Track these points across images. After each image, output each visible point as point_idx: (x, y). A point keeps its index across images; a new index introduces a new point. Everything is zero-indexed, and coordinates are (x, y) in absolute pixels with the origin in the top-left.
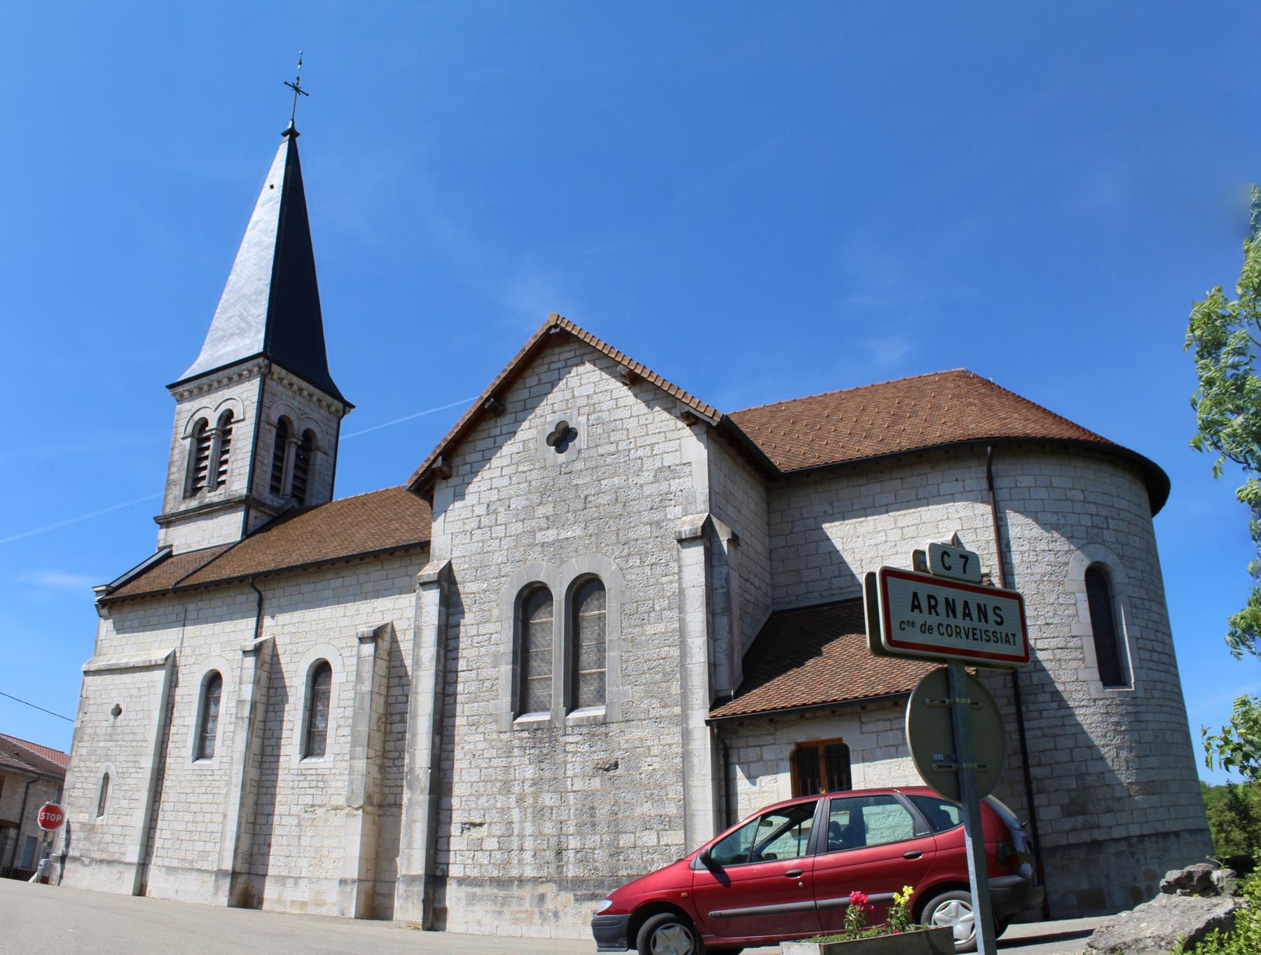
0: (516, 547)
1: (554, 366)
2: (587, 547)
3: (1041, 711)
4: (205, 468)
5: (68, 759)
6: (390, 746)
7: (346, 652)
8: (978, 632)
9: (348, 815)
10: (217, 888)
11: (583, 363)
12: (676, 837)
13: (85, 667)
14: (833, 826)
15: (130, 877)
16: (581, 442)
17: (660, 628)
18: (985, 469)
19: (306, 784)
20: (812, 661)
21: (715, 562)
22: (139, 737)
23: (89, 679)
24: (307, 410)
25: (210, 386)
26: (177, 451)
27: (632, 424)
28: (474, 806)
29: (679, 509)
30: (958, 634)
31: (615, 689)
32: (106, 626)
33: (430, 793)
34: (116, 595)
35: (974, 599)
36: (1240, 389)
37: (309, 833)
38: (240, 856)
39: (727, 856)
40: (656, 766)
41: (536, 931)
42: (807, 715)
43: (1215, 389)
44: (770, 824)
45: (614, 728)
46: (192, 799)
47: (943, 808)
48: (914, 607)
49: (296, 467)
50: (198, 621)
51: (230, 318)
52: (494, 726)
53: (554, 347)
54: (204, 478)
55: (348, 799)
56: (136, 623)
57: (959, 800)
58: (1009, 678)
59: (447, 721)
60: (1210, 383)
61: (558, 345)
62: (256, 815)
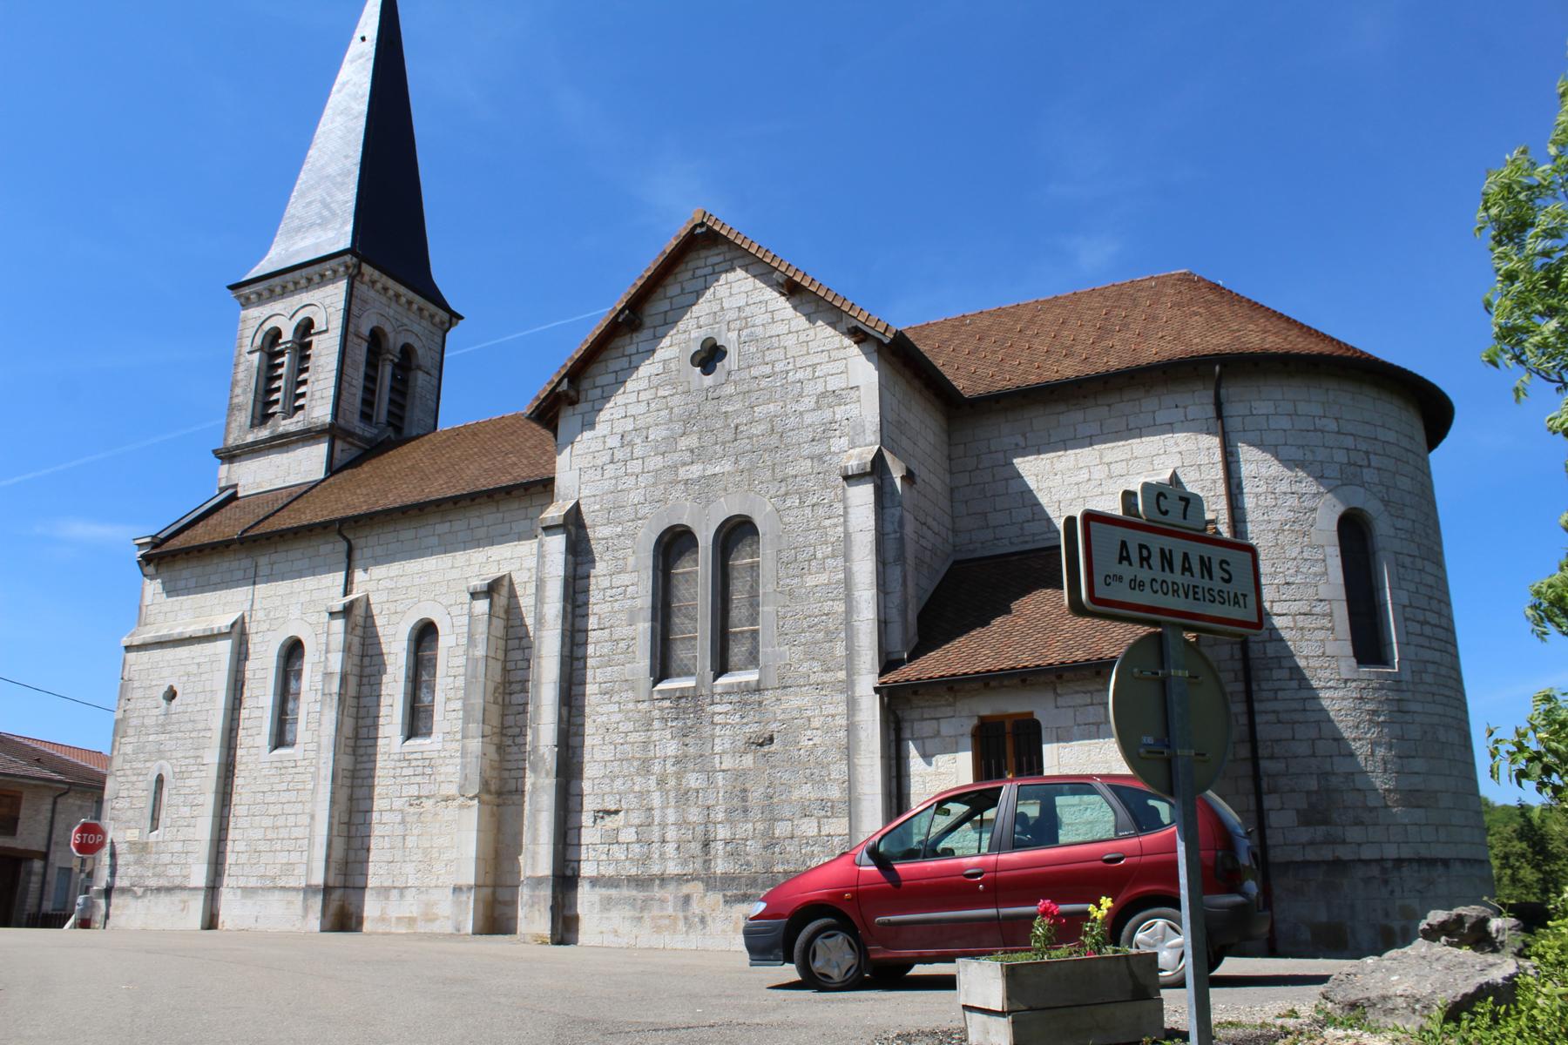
0: (654, 485)
1: (699, 272)
2: (737, 485)
3: (1276, 691)
4: (278, 390)
5: (108, 760)
6: (510, 720)
7: (455, 610)
8: (1200, 590)
9: (461, 807)
10: (306, 909)
11: (733, 269)
12: (838, 826)
13: (126, 641)
14: (1020, 818)
15: (197, 905)
16: (730, 362)
17: (823, 578)
18: (1212, 393)
19: (410, 771)
20: (1000, 619)
21: (887, 503)
22: (200, 726)
23: (132, 656)
24: (405, 321)
25: (284, 288)
26: (241, 368)
27: (790, 341)
28: (608, 789)
29: (844, 441)
30: (1175, 592)
31: (770, 650)
32: (153, 588)
33: (558, 775)
34: (165, 548)
35: (1196, 550)
36: (1553, 283)
37: (415, 832)
38: (333, 865)
39: (897, 849)
40: (817, 740)
41: (682, 941)
42: (993, 684)
43: (1517, 285)
44: (947, 812)
45: (769, 696)
46: (271, 798)
47: (1151, 802)
48: (1121, 559)
49: (392, 389)
50: (270, 578)
51: (309, 204)
52: (630, 694)
53: (702, 247)
54: (276, 402)
55: (461, 787)
56: (192, 583)
57: (1171, 793)
58: (1237, 647)
59: (576, 690)
60: (1511, 277)
61: (704, 248)
62: (350, 812)
